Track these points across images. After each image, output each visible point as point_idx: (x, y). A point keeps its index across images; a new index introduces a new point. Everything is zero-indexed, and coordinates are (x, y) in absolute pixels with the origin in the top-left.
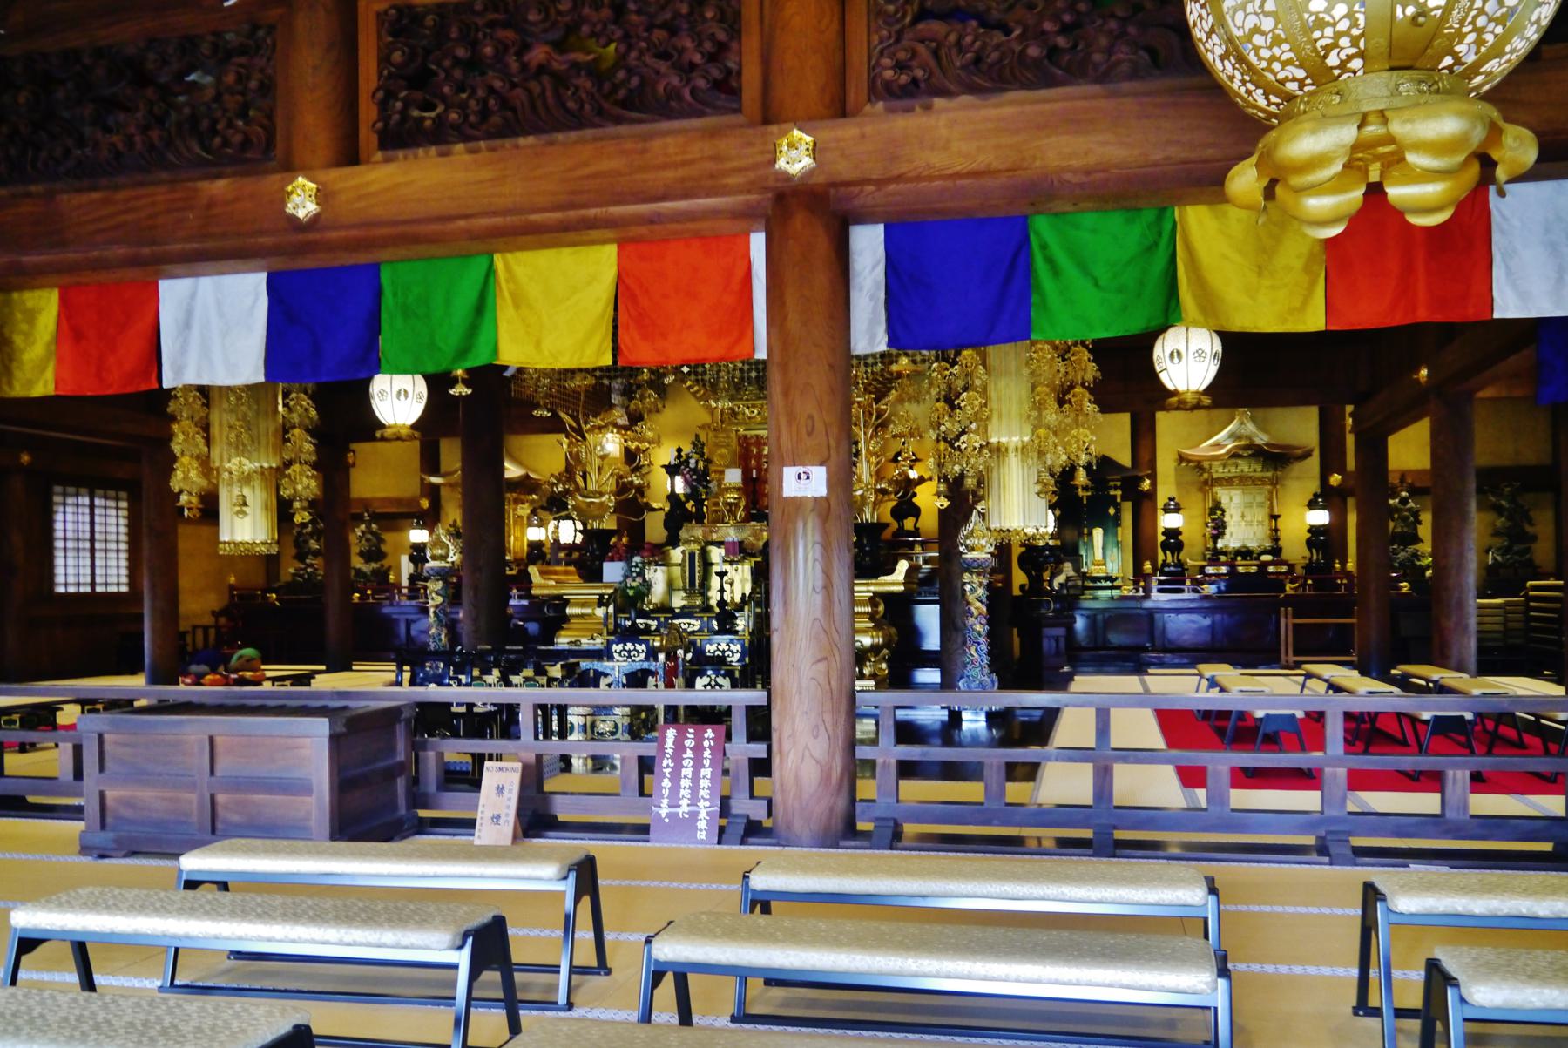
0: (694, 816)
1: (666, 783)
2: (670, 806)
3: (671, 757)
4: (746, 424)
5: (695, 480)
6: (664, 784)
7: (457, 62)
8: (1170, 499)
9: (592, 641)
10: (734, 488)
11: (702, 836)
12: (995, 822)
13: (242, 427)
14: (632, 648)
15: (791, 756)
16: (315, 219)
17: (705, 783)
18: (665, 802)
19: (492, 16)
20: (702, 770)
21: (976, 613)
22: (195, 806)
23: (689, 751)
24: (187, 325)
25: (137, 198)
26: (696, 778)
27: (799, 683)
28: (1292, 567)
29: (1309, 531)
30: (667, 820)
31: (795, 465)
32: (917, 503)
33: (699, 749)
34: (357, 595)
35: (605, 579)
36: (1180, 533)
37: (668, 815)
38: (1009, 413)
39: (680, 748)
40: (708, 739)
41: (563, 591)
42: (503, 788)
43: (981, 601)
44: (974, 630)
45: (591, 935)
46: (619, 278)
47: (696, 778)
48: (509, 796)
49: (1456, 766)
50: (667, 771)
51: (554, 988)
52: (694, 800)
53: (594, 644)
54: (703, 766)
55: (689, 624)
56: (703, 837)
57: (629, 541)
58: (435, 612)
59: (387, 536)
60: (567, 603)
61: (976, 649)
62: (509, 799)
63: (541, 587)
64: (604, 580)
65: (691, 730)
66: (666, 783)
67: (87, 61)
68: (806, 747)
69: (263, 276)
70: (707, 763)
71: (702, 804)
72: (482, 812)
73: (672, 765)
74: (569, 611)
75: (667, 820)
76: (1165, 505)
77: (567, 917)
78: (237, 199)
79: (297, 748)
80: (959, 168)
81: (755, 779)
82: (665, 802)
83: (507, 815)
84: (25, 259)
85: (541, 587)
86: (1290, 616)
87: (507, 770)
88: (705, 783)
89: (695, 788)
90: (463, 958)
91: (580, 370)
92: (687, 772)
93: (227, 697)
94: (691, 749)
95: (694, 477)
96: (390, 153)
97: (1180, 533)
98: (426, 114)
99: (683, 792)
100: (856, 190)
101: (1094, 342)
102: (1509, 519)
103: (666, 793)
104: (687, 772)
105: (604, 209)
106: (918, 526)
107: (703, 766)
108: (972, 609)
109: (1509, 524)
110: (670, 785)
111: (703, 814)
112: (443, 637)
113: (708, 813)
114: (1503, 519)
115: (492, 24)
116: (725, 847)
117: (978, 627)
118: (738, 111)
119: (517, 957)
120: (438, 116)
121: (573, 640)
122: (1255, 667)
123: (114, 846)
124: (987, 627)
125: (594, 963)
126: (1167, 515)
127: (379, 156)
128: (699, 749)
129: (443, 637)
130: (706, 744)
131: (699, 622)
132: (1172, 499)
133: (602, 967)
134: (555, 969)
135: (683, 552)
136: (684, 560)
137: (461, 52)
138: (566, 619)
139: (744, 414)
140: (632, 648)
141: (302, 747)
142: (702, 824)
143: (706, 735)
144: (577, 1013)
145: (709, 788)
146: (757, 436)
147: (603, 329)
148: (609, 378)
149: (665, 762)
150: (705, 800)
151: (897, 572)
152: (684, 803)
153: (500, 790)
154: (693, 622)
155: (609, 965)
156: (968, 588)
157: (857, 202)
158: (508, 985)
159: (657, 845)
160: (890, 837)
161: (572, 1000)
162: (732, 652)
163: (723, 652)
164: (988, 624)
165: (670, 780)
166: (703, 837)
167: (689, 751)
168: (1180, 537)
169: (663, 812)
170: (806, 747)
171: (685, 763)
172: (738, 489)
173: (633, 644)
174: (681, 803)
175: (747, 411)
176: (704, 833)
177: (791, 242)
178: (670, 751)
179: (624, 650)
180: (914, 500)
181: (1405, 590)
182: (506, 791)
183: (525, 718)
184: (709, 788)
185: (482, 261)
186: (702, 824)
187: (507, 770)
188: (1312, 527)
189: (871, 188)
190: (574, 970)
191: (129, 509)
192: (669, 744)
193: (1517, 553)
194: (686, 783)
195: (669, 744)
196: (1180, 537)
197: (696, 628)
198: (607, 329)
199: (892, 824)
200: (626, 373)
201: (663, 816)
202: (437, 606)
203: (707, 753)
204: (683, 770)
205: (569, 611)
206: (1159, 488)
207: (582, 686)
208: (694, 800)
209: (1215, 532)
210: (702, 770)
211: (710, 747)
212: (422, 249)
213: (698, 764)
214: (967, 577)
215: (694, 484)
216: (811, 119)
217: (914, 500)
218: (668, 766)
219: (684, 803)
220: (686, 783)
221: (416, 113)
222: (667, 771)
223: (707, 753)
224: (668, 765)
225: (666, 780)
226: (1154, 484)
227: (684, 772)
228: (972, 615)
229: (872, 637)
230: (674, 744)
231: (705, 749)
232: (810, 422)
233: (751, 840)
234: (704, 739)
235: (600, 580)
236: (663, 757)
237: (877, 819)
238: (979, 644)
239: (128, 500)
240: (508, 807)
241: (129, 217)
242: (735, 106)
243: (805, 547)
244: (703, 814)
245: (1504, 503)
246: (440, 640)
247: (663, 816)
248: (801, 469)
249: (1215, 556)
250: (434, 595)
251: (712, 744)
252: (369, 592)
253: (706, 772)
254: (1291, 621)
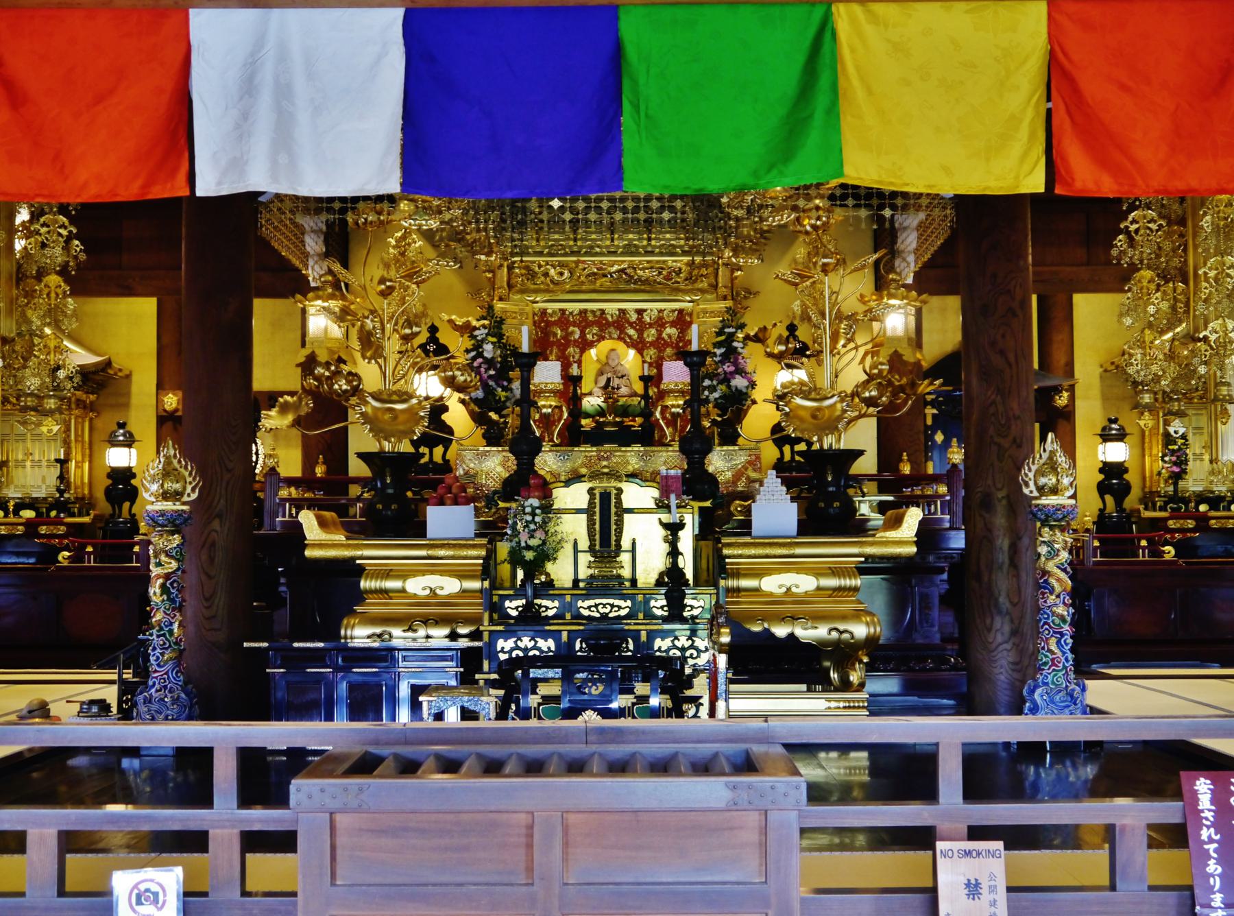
4: (547, 291)
5: (490, 377)
8: (1111, 421)
9: (410, 634)
10: (551, 391)
14: (531, 644)
21: (1058, 588)
24: (248, 86)
32: (449, 422)
42: (977, 884)
43: (1064, 570)
44: (1054, 613)
46: (1052, 56)
48: (992, 897)
53: (414, 640)
55: (612, 606)
57: (328, 472)
60: (359, 571)
61: (1058, 643)
62: (993, 903)
63: (321, 546)
64: (429, 535)
73: (1217, 837)
76: (1104, 429)
79: (731, 829)
81: (248, 855)
85: (321, 546)
87: (979, 854)
91: (366, 198)
93: (376, 743)
95: (492, 372)
101: (85, 206)
106: (447, 458)
108: (1053, 581)
110: (1220, 870)
112: (176, 626)
117: (1061, 610)
121: (378, 630)
124: (1071, 610)
126: (1109, 445)
129: (176, 626)
132: (1115, 421)
135: (591, 491)
136: (591, 503)
138: (360, 596)
139: (546, 274)
140: (531, 644)
146: (563, 311)
148: (893, 207)
149: (1205, 834)
151: (905, 525)
153: (973, 889)
156: (1043, 550)
162: (697, 649)
163: (683, 650)
164: (1072, 605)
165: (1219, 862)
168: (1126, 476)
172: (555, 393)
173: (533, 639)
175: (552, 272)
178: (1209, 815)
179: (517, 648)
181: (1167, 557)
182: (985, 890)
183: (225, 772)
185: (819, 11)
187: (979, 854)
188: (1105, 464)
196: (1126, 476)
197: (623, 613)
202: (167, 576)
205: (365, 584)
206: (1078, 403)
207: (971, 712)
209: (1176, 469)
214: (1046, 533)
215: (491, 383)
217: (444, 417)
218: (1211, 841)
224: (1210, 837)
226: (1072, 398)
228: (1052, 591)
229: (867, 624)
230: (1212, 803)
235: (749, 534)
238: (1062, 635)
246: (171, 632)
249: (1177, 500)
250: (163, 558)
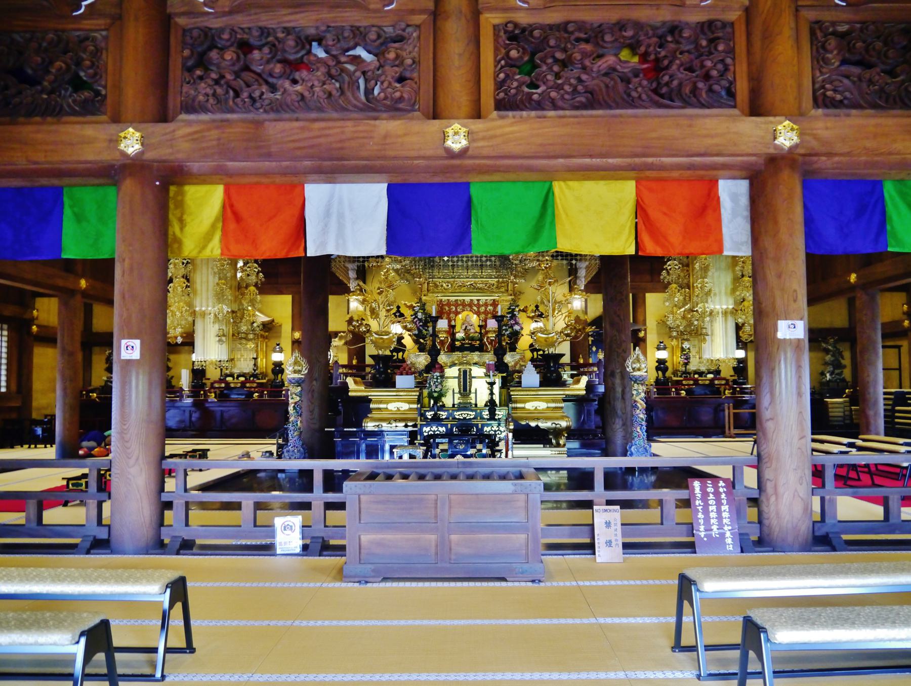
0: (723, 535)
1: (700, 516)
2: (706, 530)
3: (701, 499)
6: (699, 516)
7: (556, 60)
11: (730, 548)
12: (897, 532)
13: (224, 284)
14: (436, 429)
15: (785, 496)
16: (463, 153)
17: (725, 515)
18: (702, 528)
19: (577, 34)
20: (723, 507)
22: (433, 544)
23: (711, 495)
25: (329, 128)
26: (719, 512)
27: (184, 456)
28: (727, 381)
29: (657, 362)
30: (705, 539)
31: (786, 319)
33: (717, 494)
34: (257, 394)
35: (397, 386)
36: (666, 362)
37: (705, 536)
38: (720, 292)
39: (705, 494)
40: (722, 487)
41: (370, 394)
42: (610, 523)
45: (182, 623)
47: (719, 512)
49: (247, 499)
50: (700, 508)
51: (154, 665)
52: (721, 526)
54: (722, 504)
56: (731, 549)
58: (294, 407)
59: (172, 357)
60: (370, 401)
62: (616, 530)
65: (709, 482)
66: (700, 516)
67: (281, 35)
68: (796, 491)
69: (385, 186)
70: (724, 502)
71: (726, 528)
72: (598, 539)
74: (372, 406)
75: (705, 539)
77: (164, 613)
78: (405, 135)
80: (882, 151)
82: (702, 528)
83: (616, 540)
84: (230, 164)
86: (731, 408)
87: (610, 511)
88: (725, 515)
89: (720, 518)
90: (79, 650)
92: (713, 508)
94: (712, 493)
96: (502, 113)
97: (666, 362)
98: (534, 91)
99: (712, 521)
100: (815, 159)
102: (832, 356)
103: (701, 521)
104: (713, 508)
105: (658, 159)
107: (722, 504)
109: (833, 359)
110: (703, 516)
111: (728, 534)
113: (732, 534)
114: (829, 356)
115: (578, 40)
116: (744, 554)
118: (735, 107)
119: (117, 642)
120: (543, 92)
122: (710, 437)
123: (373, 574)
125: (183, 644)
127: (495, 114)
128: (717, 494)
129: (299, 422)
130: (721, 490)
131: (474, 413)
133: (190, 648)
134: (155, 650)
135: (459, 370)
136: (460, 374)
137: (559, 55)
138: (370, 411)
139: (442, 286)
141: (518, 501)
142: (729, 541)
143: (720, 485)
144: (167, 679)
145: (729, 518)
146: (448, 300)
147: (627, 231)
148: (576, 260)
149: (697, 503)
150: (728, 525)
151: (581, 383)
152: (715, 528)
153: (608, 524)
154: (470, 413)
155: (195, 645)
156: (634, 392)
157: (816, 166)
158: (111, 663)
159: (700, 555)
160: (319, 548)
161: (165, 674)
163: (495, 431)
166: (731, 549)
167: (711, 495)
169: (702, 534)
170: (796, 491)
171: (710, 502)
174: (712, 527)
176: (731, 546)
177: (781, 186)
178: (699, 495)
180: (403, 341)
181: (683, 395)
182: (612, 525)
183: (318, 479)
184: (729, 518)
186: (729, 541)
187: (610, 511)
189: (824, 158)
190: (168, 650)
191: (8, 336)
192: (697, 490)
193: (837, 374)
194: (713, 515)
195: (697, 490)
197: (472, 417)
198: (630, 232)
199: (321, 540)
200: (569, 258)
201: (702, 536)
202: (296, 403)
203: (723, 496)
204: (710, 507)
208: (721, 526)
210: (723, 507)
211: (724, 492)
212: (497, 177)
213: (719, 503)
216: (791, 115)
218: (700, 505)
219: (715, 528)
220: (713, 515)
221: (526, 90)
222: (700, 508)
223: (723, 496)
225: (700, 514)
226: (646, 334)
227: (711, 508)
230: (700, 490)
231: (721, 493)
232: (795, 294)
233: (325, 553)
234: (719, 487)
235: (394, 387)
236: (695, 499)
237: (313, 538)
239: (8, 330)
240: (616, 535)
241: (322, 140)
242: (732, 104)
243: (786, 367)
244: (728, 534)
245: (830, 347)
246: (297, 424)
247: (702, 536)
248: (790, 322)
250: (294, 396)
251: (725, 490)
252: (265, 392)
253: (725, 508)
254: (732, 411)
